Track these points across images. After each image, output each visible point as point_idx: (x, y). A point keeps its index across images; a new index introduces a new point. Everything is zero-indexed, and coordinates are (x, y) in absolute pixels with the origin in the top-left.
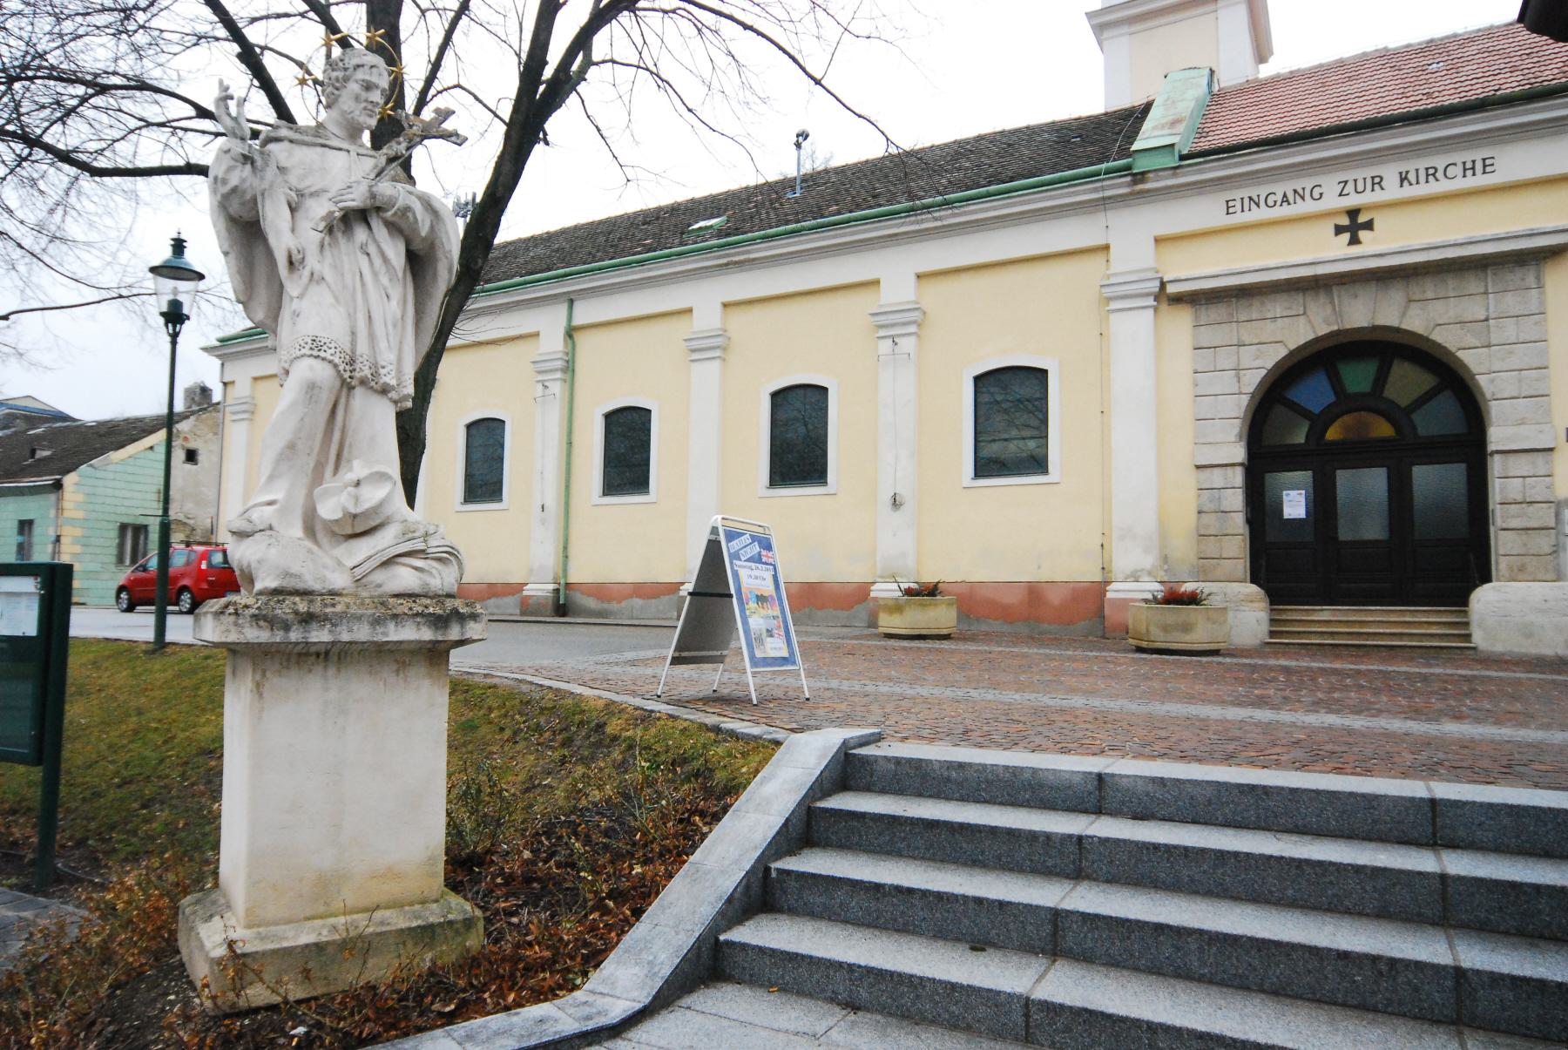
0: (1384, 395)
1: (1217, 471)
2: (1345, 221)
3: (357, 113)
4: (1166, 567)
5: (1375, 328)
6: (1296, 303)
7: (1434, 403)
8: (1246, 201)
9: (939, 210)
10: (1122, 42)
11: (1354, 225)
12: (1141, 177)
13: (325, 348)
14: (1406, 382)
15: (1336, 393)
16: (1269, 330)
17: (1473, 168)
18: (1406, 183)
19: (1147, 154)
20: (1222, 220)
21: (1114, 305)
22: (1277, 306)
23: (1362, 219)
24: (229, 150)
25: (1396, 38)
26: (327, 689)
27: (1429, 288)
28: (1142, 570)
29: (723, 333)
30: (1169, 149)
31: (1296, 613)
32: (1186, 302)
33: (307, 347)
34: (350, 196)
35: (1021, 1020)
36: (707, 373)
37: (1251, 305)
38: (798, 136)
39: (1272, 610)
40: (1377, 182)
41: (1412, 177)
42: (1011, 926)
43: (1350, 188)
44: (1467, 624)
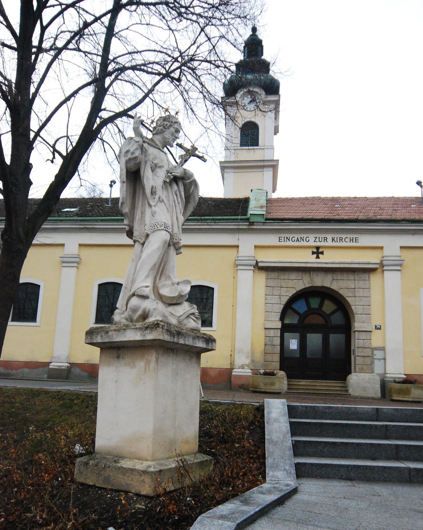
0: (323, 309)
1: (272, 331)
2: (315, 250)
3: (171, 140)
4: (253, 364)
5: (323, 287)
6: (299, 275)
7: (335, 315)
8: (285, 238)
9: (211, 222)
10: (230, 175)
11: (318, 252)
12: (252, 224)
13: (168, 228)
14: (328, 307)
15: (308, 308)
16: (290, 283)
17: (353, 240)
18: (334, 241)
19: (255, 216)
20: (277, 243)
21: (239, 267)
22: (293, 276)
23: (320, 250)
24: (139, 142)
25: (323, 196)
26: (173, 364)
27: (339, 276)
28: (245, 365)
29: (78, 257)
30: (263, 216)
31: (295, 382)
32: (264, 270)
33: (163, 227)
34: (177, 171)
35: (408, 476)
36: (70, 273)
37: (285, 274)
38: (111, 182)
39: (288, 381)
40: (326, 239)
41: (335, 239)
42: (383, 452)
43: (317, 239)
44: (346, 387)
